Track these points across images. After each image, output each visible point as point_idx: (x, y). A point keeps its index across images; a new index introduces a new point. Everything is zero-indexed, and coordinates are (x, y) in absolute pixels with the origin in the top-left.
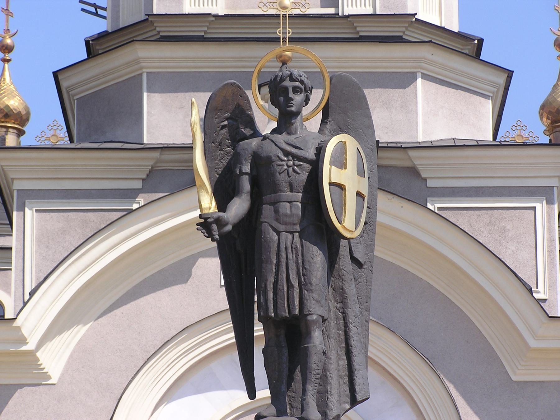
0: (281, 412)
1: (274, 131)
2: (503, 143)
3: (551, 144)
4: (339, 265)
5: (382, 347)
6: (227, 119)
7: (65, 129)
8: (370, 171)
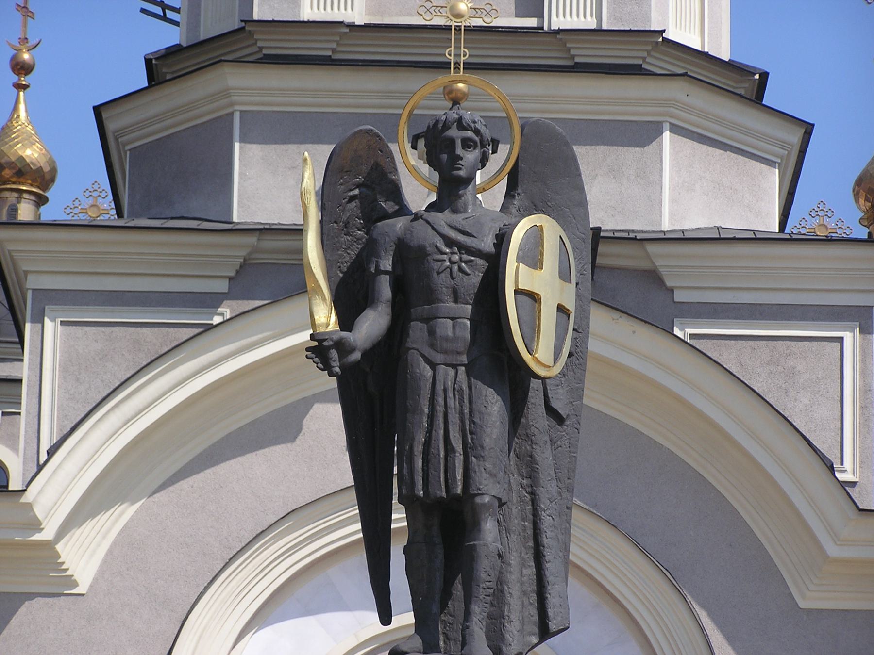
0: (430, 644)
1: (431, 207)
2: (794, 237)
3: (872, 240)
4: (527, 418)
5: (591, 546)
6: (358, 186)
7: (110, 197)
8: (580, 273)
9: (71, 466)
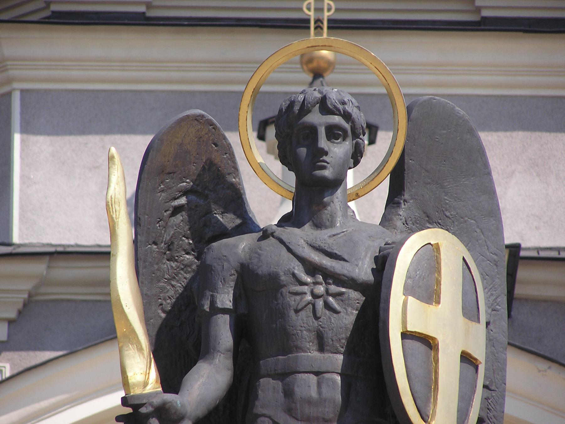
1: (286, 221)
6: (186, 193)
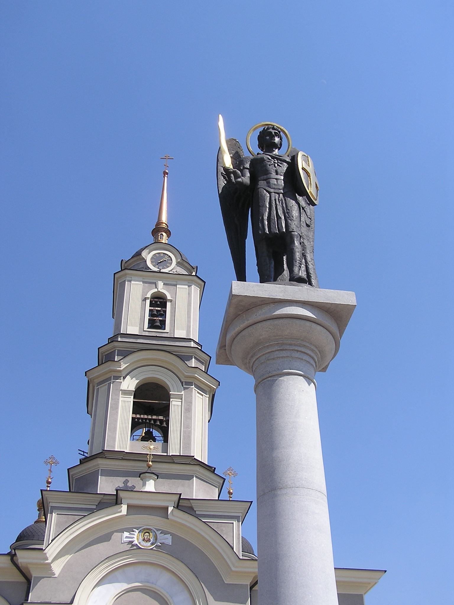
9: (56, 544)
